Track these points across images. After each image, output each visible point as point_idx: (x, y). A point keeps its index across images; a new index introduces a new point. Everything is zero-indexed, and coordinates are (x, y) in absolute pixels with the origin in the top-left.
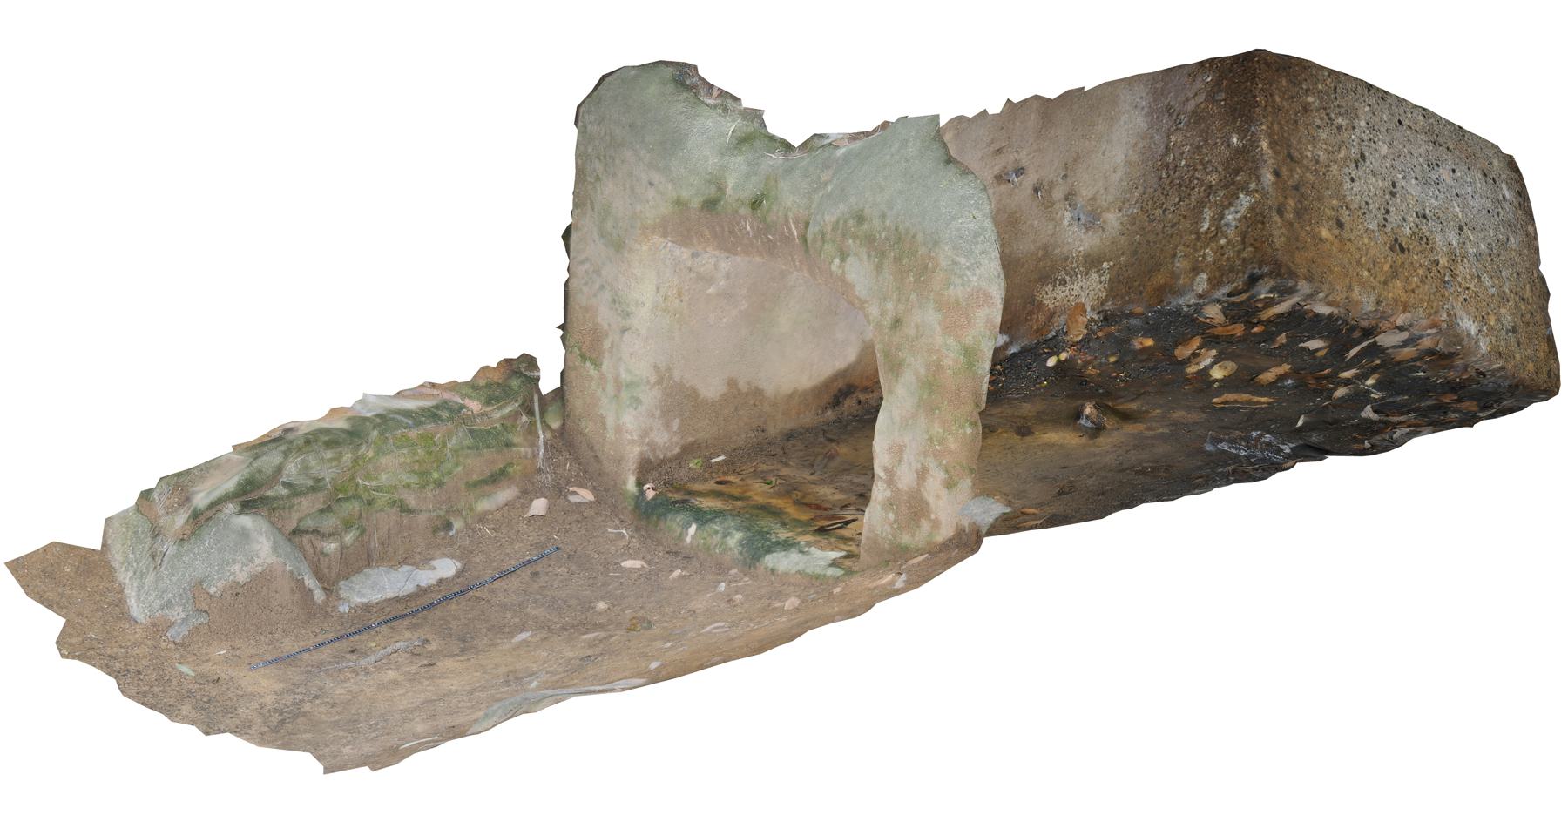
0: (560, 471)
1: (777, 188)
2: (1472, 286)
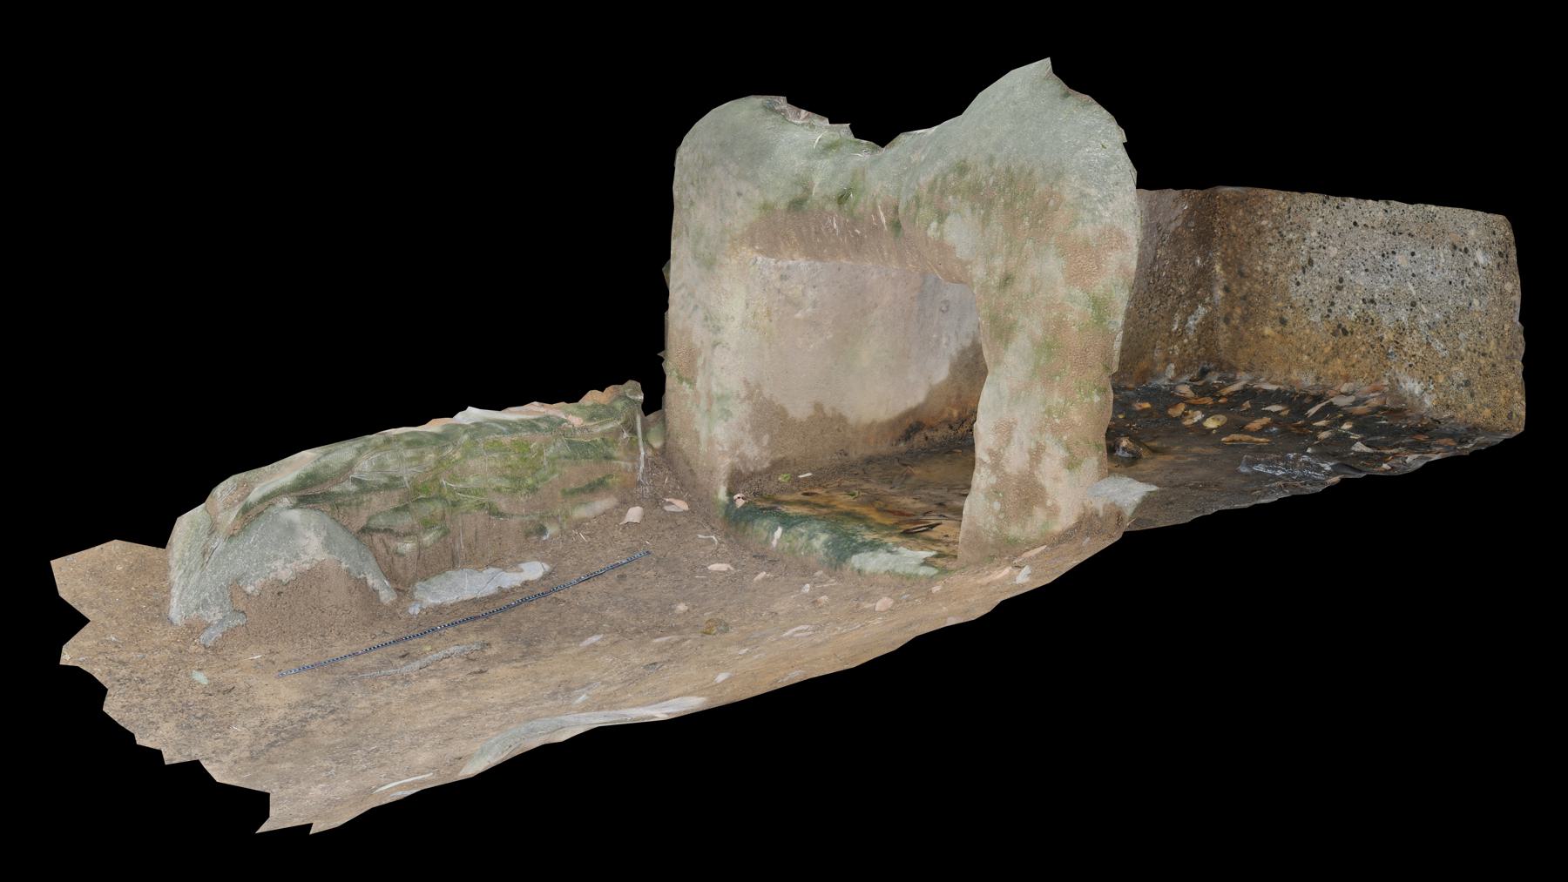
0: (658, 484)
1: (864, 180)
2: (1419, 353)
